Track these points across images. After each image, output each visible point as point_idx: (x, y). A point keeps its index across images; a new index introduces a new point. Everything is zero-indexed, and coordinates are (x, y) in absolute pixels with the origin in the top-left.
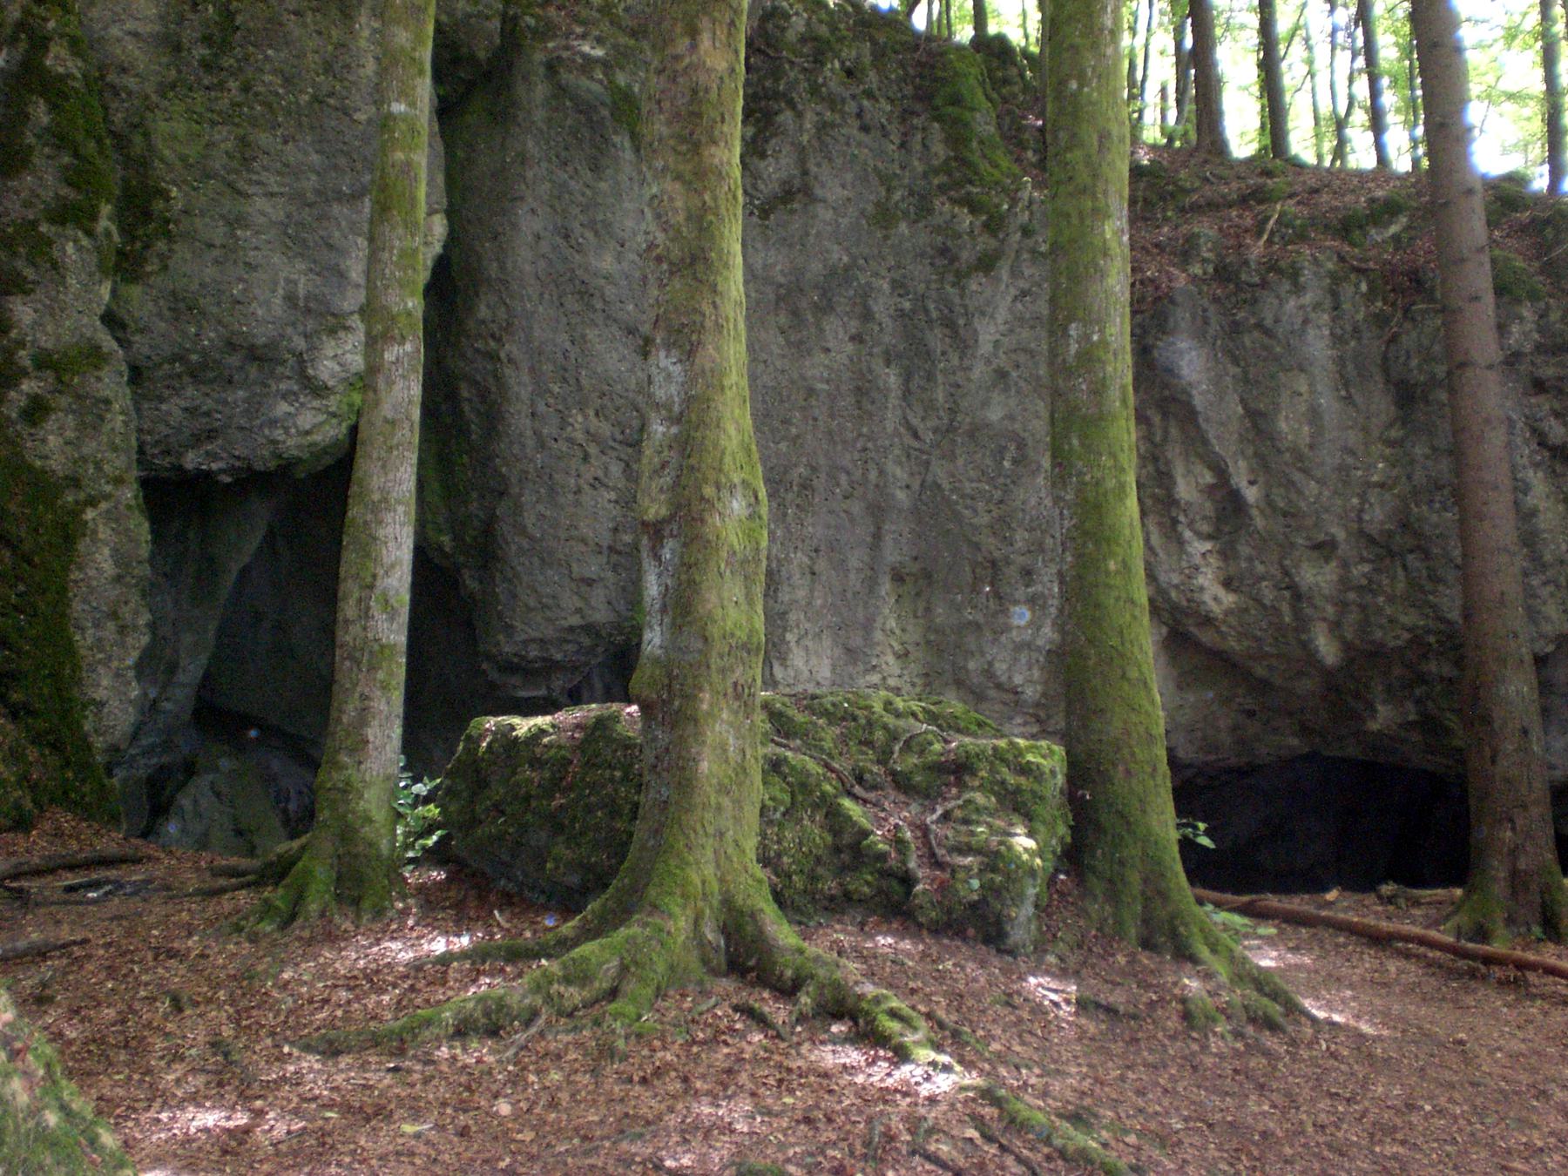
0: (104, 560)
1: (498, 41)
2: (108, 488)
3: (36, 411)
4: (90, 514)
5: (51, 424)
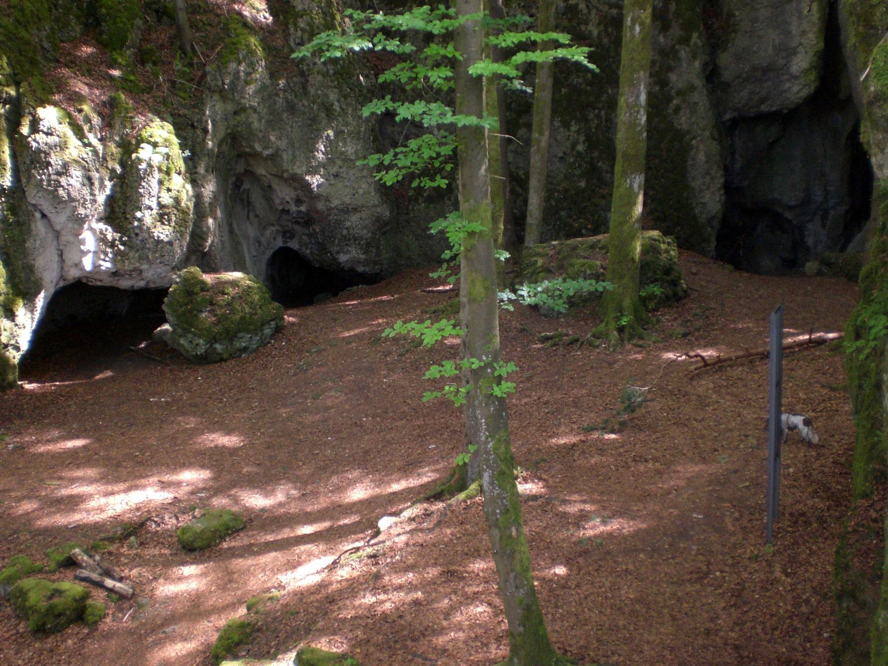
0: (701, 157)
1: (20, 512)
2: (700, 132)
3: (677, 109)
4: (694, 142)
5: (682, 113)
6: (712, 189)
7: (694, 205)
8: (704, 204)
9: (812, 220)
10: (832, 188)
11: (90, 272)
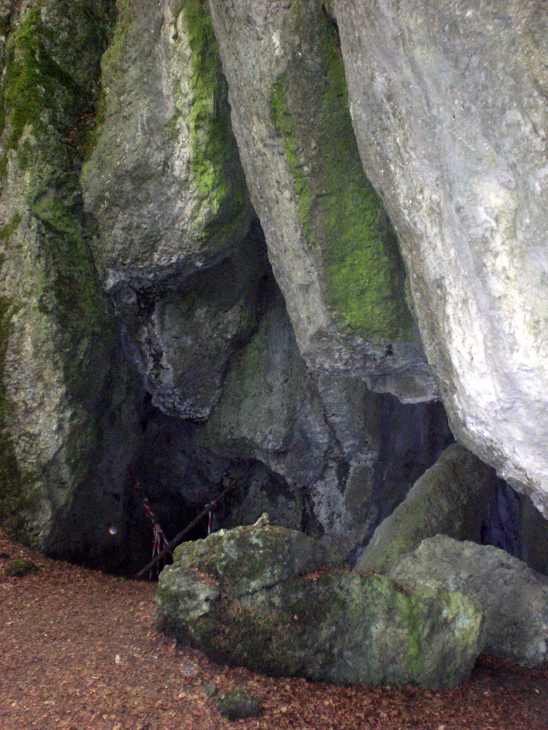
0: (28, 347)
2: (24, 300)
6: (48, 409)
7: (14, 437)
8: (33, 437)
9: (322, 477)
10: (338, 420)
11: (117, 528)
